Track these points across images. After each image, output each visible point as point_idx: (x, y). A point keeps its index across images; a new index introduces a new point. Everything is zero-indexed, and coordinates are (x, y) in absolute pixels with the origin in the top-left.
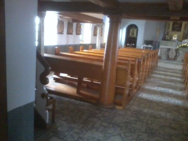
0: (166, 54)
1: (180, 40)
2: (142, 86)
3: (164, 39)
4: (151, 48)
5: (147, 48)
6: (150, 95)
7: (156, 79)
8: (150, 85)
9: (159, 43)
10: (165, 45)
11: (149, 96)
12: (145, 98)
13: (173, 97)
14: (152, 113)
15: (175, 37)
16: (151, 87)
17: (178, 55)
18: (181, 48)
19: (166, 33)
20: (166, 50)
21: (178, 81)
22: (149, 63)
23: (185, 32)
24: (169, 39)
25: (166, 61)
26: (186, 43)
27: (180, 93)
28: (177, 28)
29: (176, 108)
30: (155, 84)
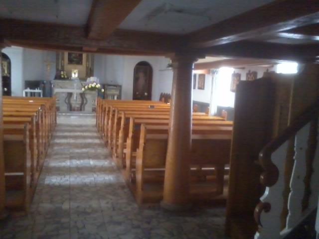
0: (66, 102)
1: (82, 79)
2: (45, 164)
3: (58, 77)
4: (39, 94)
5: (32, 94)
6: (63, 177)
7: (62, 147)
8: (56, 159)
9: (51, 84)
10: (61, 88)
11: (61, 179)
12: (57, 184)
13: (103, 171)
14: (78, 207)
15: (75, 74)
16: (60, 162)
17: (85, 102)
18: (88, 92)
19: (60, 68)
20: (65, 96)
21: (96, 144)
22: (47, 121)
23: (89, 65)
24: (66, 77)
25: (68, 114)
26: (94, 82)
27: (105, 163)
28: (76, 61)
29: (109, 188)
30: (64, 156)
